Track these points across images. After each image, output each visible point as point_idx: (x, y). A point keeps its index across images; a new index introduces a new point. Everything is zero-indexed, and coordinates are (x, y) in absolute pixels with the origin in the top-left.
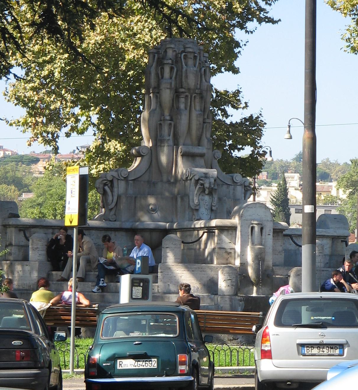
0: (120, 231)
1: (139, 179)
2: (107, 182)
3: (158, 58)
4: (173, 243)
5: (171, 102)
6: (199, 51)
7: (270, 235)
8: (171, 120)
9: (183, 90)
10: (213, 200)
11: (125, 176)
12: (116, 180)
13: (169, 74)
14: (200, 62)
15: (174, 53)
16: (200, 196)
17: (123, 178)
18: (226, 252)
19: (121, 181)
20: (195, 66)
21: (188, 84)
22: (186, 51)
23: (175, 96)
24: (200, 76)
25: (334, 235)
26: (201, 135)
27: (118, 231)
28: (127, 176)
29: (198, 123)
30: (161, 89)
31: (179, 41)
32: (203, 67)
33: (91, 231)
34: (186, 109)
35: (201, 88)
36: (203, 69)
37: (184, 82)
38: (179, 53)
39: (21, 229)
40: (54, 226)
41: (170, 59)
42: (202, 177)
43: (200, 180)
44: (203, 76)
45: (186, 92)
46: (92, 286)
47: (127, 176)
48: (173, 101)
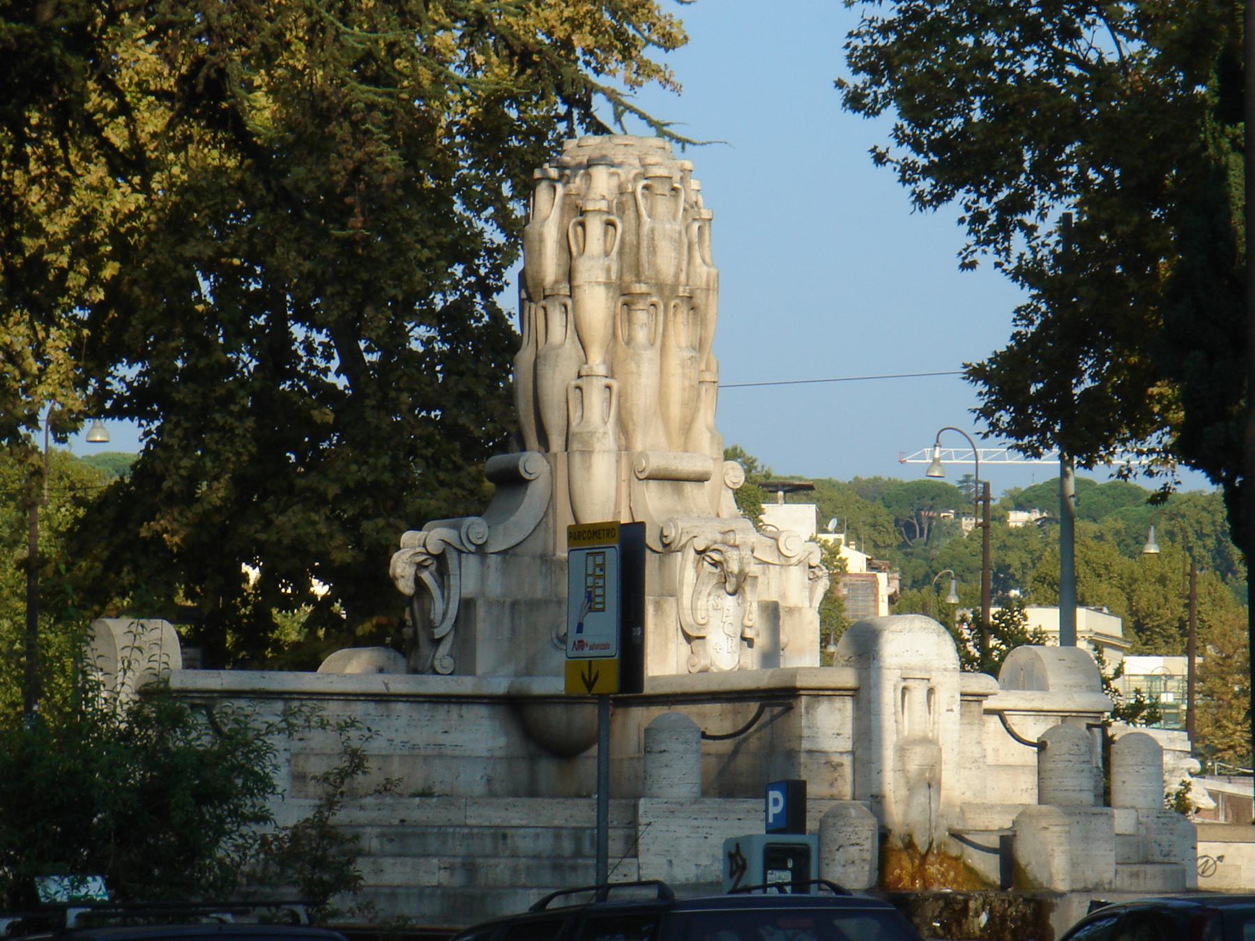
0: (472, 703)
1: (519, 550)
2: (425, 560)
3: (567, 195)
4: (680, 740)
5: (610, 323)
6: (681, 174)
7: (951, 710)
8: (611, 374)
9: (643, 288)
10: (745, 611)
11: (480, 542)
12: (455, 554)
13: (602, 242)
14: (687, 206)
15: (614, 181)
16: (711, 598)
17: (472, 548)
18: (828, 763)
19: (470, 555)
20: (674, 218)
21: (657, 272)
22: (649, 175)
23: (619, 305)
24: (686, 247)
25: (1068, 708)
26: (693, 420)
27: (467, 703)
28: (486, 543)
29: (687, 383)
30: (578, 287)
31: (626, 145)
32: (695, 220)
33: (393, 705)
34: (652, 344)
35: (690, 283)
36: (696, 226)
37: (646, 265)
38: (629, 181)
39: (198, 701)
40: (290, 693)
41: (604, 198)
42: (715, 543)
43: (714, 550)
44: (696, 247)
45: (648, 294)
46: (440, 868)
47: (484, 540)
48: (614, 317)
